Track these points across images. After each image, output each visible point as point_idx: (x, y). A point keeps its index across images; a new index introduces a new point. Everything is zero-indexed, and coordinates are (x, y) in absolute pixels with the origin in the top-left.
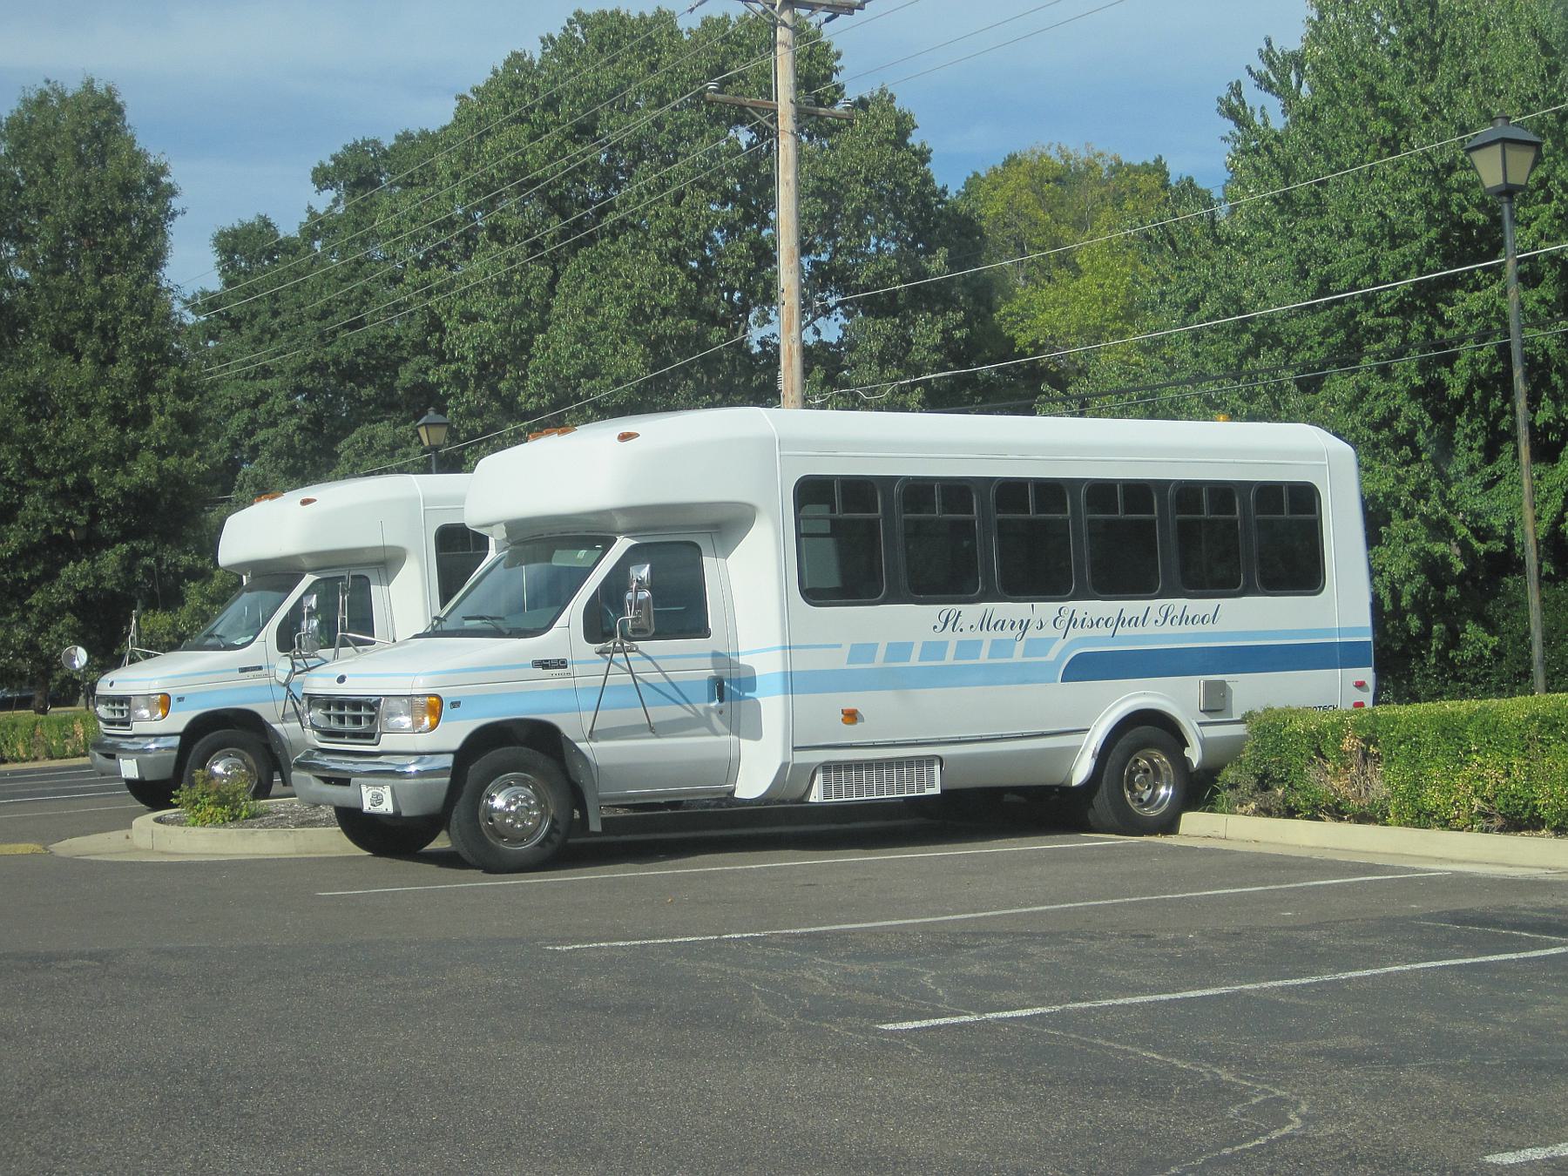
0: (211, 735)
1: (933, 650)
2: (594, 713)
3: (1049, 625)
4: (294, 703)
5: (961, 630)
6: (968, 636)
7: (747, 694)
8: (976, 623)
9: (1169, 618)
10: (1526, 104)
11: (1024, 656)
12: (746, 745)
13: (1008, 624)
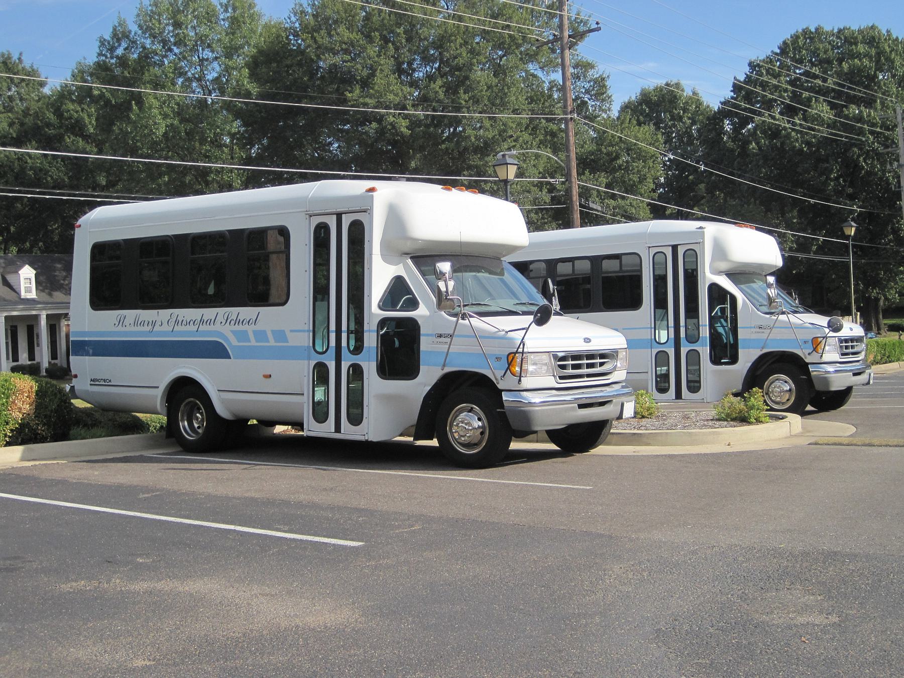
0: (766, 383)
2: (504, 372)
3: (165, 323)
9: (229, 321)
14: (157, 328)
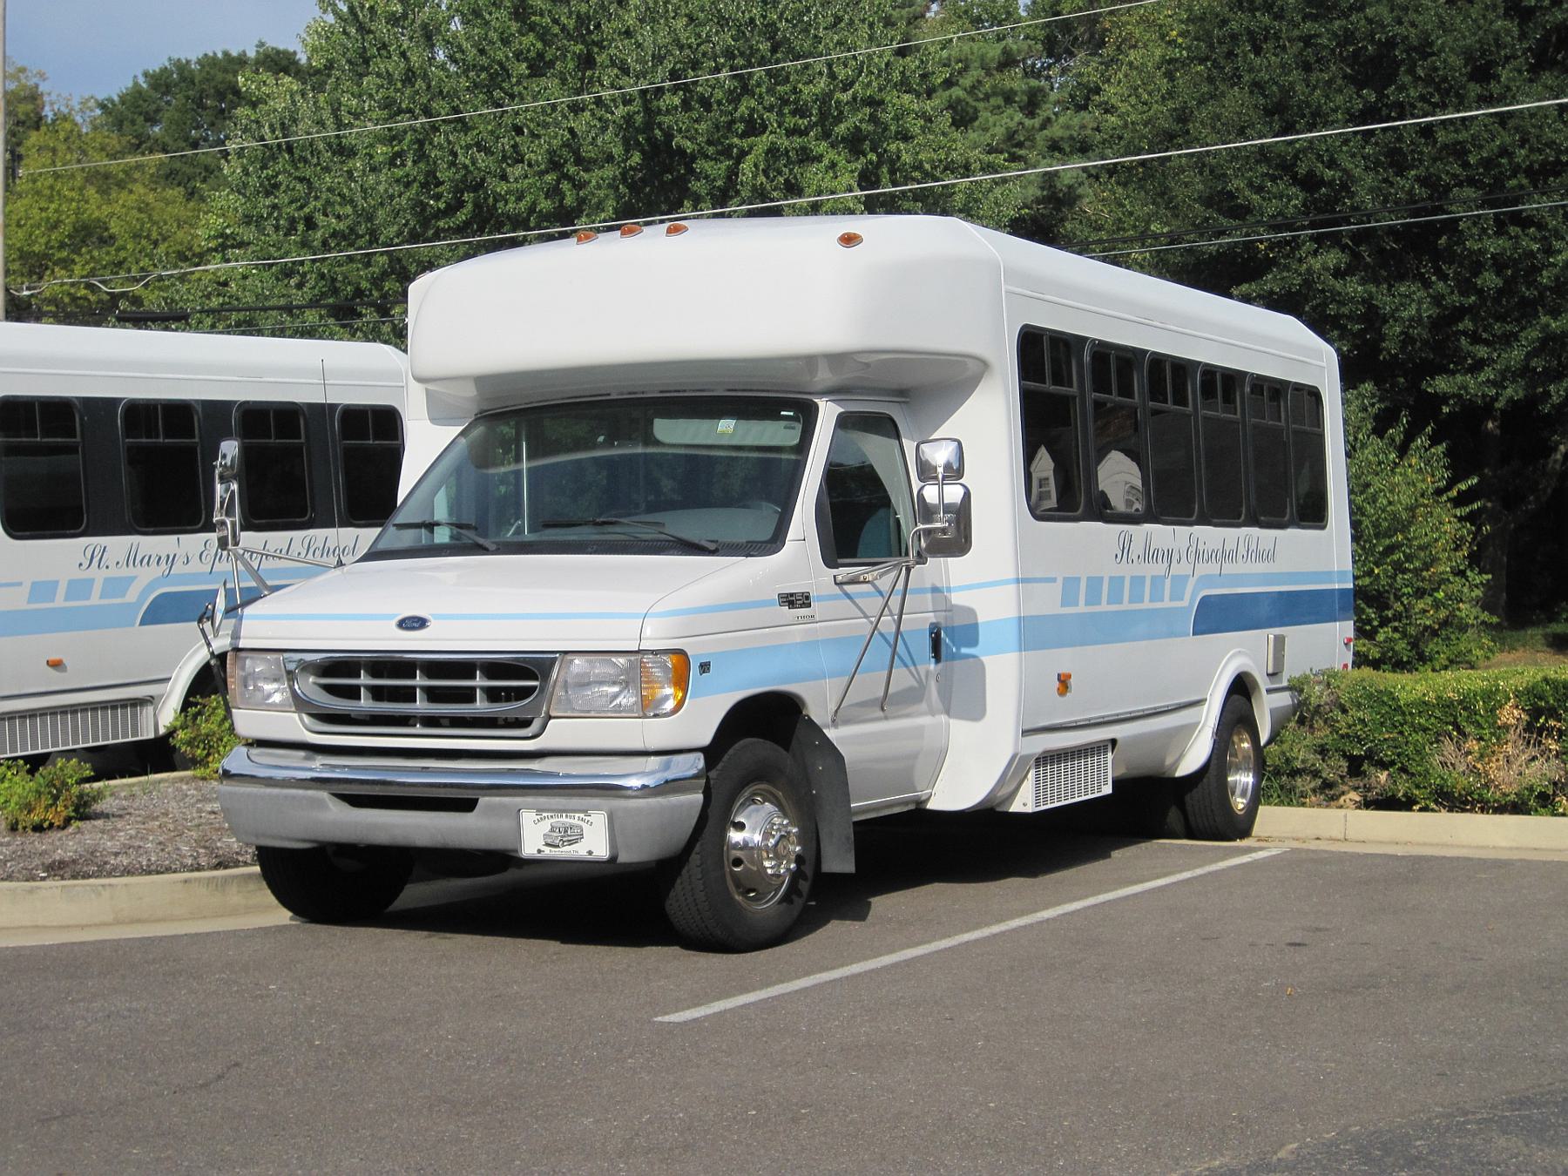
1: (79, 588)
2: (885, 673)
4: (918, 673)
5: (107, 567)
6: (114, 572)
7: (964, 650)
8: (122, 559)
10: (742, 28)
11: (29, 602)
12: (960, 730)
13: (154, 560)
14: (178, 568)
